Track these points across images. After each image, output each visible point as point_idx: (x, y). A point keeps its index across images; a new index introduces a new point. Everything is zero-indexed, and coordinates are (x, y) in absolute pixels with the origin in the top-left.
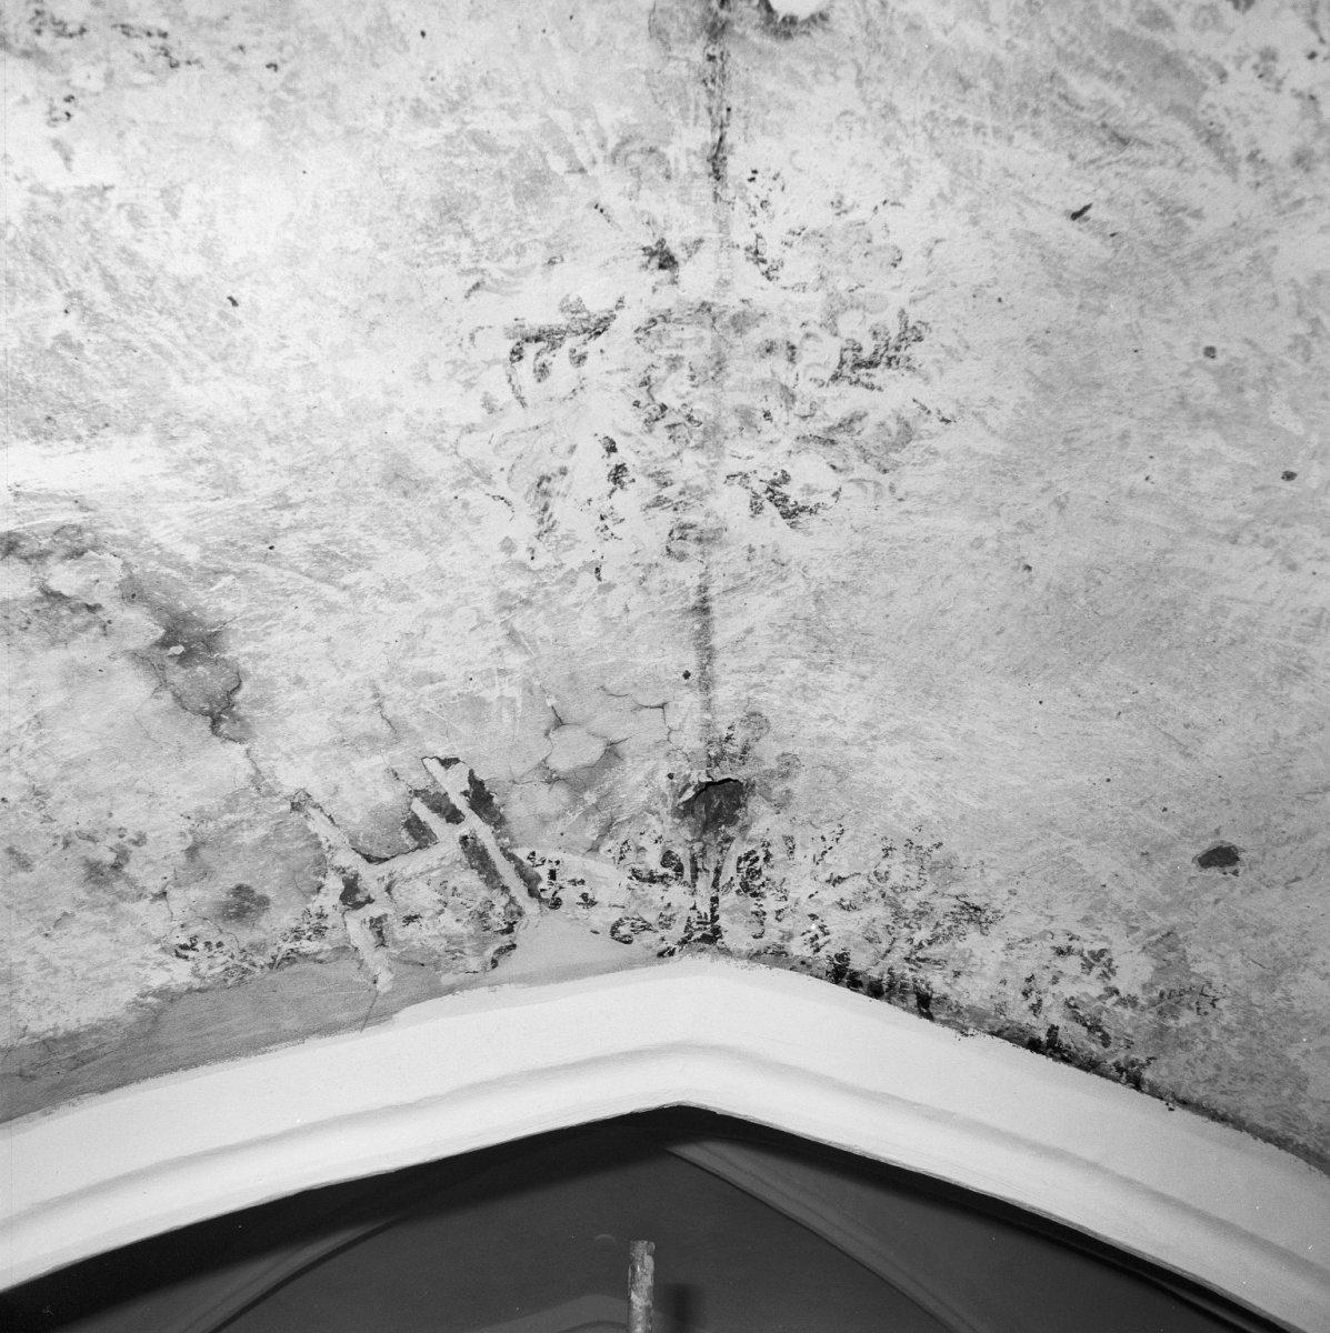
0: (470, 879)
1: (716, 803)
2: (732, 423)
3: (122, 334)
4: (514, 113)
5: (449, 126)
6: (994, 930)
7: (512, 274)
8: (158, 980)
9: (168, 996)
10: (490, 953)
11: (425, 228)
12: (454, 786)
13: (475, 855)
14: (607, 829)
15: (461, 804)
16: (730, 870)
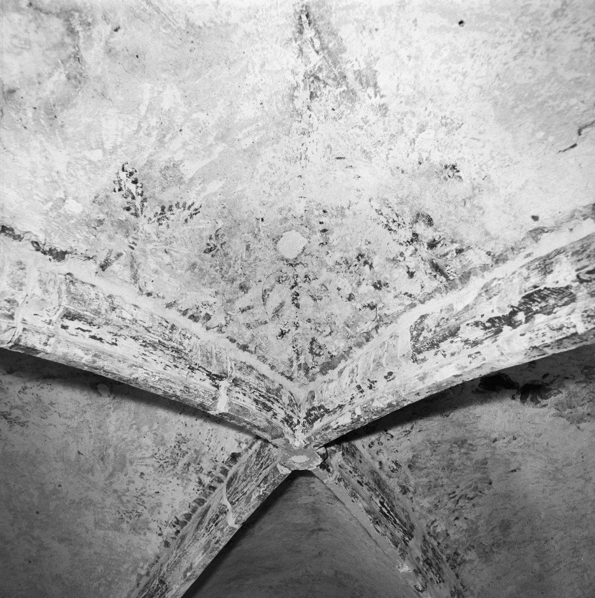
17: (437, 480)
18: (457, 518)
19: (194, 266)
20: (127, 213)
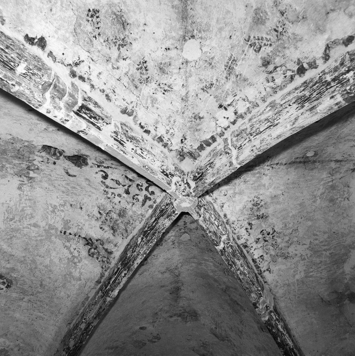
3: (333, 247)
4: (319, 189)
5: (318, 198)
7: (348, 193)
11: (334, 204)
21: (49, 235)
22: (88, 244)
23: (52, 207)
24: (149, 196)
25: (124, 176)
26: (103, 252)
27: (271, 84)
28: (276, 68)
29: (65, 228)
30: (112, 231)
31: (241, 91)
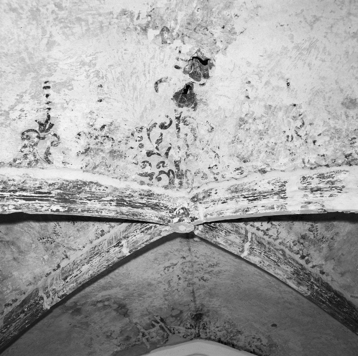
0: (161, 331)
1: (198, 317)
2: (195, 272)
6: (243, 335)
8: (116, 350)
9: (117, 352)
10: (164, 341)
12: (158, 319)
13: (162, 328)
14: (181, 322)
15: (159, 321)
16: (201, 326)
17: (267, 146)
18: (314, 142)
19: (78, 230)
20: (53, 244)
21: (36, 67)
22: (41, 124)
23: (91, 61)
24: (154, 177)
25: (170, 146)
26: (40, 150)
27: (292, 244)
28: (302, 244)
29: (55, 85)
30: (83, 150)
31: (283, 228)
